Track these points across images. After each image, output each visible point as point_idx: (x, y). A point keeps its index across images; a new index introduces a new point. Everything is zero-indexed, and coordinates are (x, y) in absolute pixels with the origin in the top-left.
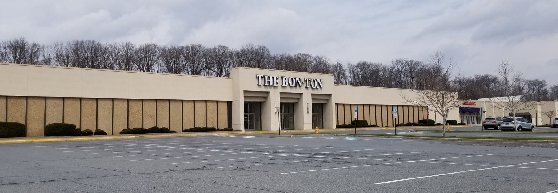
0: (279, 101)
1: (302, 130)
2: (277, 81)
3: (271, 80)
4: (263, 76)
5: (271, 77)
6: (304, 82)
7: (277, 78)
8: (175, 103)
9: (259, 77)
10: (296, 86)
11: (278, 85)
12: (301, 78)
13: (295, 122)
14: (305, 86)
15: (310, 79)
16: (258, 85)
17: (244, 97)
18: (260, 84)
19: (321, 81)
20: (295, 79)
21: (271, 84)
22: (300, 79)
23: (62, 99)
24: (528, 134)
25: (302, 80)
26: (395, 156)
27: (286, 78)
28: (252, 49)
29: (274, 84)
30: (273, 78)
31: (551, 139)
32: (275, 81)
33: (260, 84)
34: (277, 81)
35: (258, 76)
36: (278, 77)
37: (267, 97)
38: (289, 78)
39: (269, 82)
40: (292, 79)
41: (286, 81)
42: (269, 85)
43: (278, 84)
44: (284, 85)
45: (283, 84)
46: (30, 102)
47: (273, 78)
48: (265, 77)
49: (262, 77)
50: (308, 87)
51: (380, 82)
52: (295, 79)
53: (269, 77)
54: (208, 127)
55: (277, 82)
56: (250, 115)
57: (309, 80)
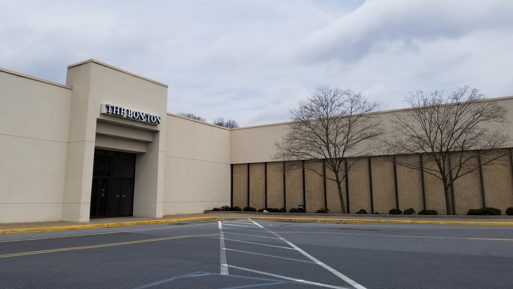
0: (95, 145)
1: (147, 218)
2: (124, 112)
3: (118, 110)
4: (112, 106)
7: (124, 110)
17: (98, 135)
19: (159, 118)
22: (142, 114)
24: (37, 224)
25: (144, 115)
27: (132, 111)
28: (465, 130)
30: (120, 109)
31: (201, 222)
34: (124, 112)
35: (147, 114)
37: (150, 142)
39: (117, 112)
41: (131, 113)
43: (124, 114)
46: (485, 159)
47: (120, 109)
51: (473, 151)
53: (117, 108)
54: (269, 207)
55: (123, 113)
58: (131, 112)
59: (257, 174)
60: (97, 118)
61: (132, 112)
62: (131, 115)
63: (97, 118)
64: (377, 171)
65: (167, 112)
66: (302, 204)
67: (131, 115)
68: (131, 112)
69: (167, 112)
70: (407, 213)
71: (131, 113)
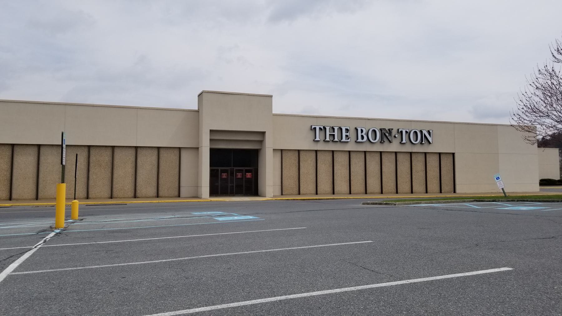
2: (348, 134)
4: (322, 127)
5: (336, 129)
6: (397, 136)
7: (347, 130)
8: (134, 158)
9: (315, 128)
10: (382, 142)
11: (349, 140)
12: (431, 131)
13: (334, 165)
14: (399, 140)
15: (408, 131)
16: (314, 140)
18: (317, 139)
19: (429, 133)
20: (421, 132)
21: (336, 139)
23: (178, 150)
26: (14, 260)
29: (342, 138)
30: (341, 129)
32: (344, 134)
33: (317, 139)
34: (348, 134)
35: (400, 130)
36: (349, 128)
38: (369, 130)
40: (416, 132)
41: (363, 134)
42: (324, 141)
43: (349, 139)
44: (360, 140)
45: (357, 139)
48: (325, 128)
49: (320, 129)
50: (404, 141)
52: (421, 132)
55: (347, 136)
56: (221, 170)
57: (406, 132)
58: (362, 131)
59: (168, 159)
60: (265, 132)
61: (364, 132)
62: (363, 137)
63: (265, 132)
64: (18, 159)
65: (273, 113)
66: (61, 144)
67: (363, 137)
68: (362, 131)
69: (273, 113)
70: (281, 251)
71: (363, 134)
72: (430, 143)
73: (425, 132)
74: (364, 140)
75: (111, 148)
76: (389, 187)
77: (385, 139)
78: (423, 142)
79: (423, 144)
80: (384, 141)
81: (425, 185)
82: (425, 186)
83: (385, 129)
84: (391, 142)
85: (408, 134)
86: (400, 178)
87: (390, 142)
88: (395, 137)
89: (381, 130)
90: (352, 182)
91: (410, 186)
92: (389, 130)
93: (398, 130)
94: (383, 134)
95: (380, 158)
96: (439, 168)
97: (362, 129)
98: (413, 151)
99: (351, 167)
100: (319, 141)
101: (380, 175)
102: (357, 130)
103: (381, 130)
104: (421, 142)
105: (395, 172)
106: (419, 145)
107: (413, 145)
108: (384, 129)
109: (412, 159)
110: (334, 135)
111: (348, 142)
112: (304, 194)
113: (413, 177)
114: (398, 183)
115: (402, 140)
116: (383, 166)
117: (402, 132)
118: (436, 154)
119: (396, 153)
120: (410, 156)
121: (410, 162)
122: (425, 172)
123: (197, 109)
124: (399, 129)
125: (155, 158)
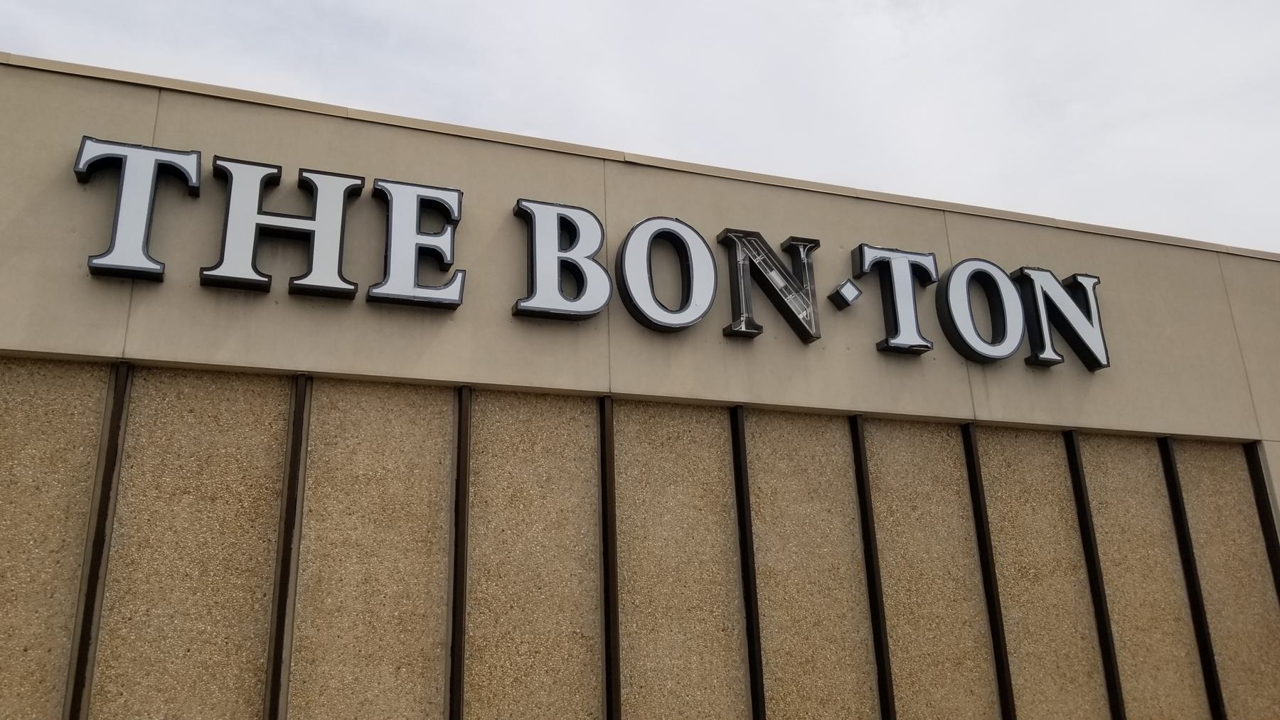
5: (331, 194)
6: (849, 292)
12: (1087, 283)
15: (927, 262)
19: (1074, 288)
20: (1022, 281)
34: (442, 242)
35: (870, 256)
36: (451, 199)
41: (578, 254)
50: (908, 336)
52: (1022, 281)
57: (920, 275)
58: (568, 232)
62: (572, 277)
67: (572, 277)
68: (568, 232)
72: (1090, 362)
73: (1045, 283)
74: (588, 303)
75: (104, 374)
76: (823, 703)
77: (762, 313)
78: (1048, 354)
79: (1048, 364)
80: (750, 323)
81: (1099, 678)
82: (1103, 691)
83: (757, 235)
84: (813, 331)
85: (932, 288)
86: (908, 629)
87: (804, 336)
88: (838, 301)
89: (727, 242)
90: (474, 671)
91: (994, 687)
92: (791, 248)
93: (859, 253)
94: (744, 281)
95: (729, 458)
96: (1174, 548)
97: (576, 216)
98: (984, 415)
99: (476, 529)
100: (150, 279)
101: (737, 602)
102: (524, 217)
103: (727, 242)
104: (1027, 353)
105: (863, 576)
106: (1018, 376)
107: (976, 373)
108: (751, 237)
109: (984, 471)
110: (304, 240)
111: (447, 308)
112: (1152, 439)
113: (1010, 616)
114: (895, 668)
115: (892, 326)
116: (757, 527)
117: (883, 269)
118: (1140, 449)
119: (855, 423)
120: (727, 434)
121: (967, 499)
122: (1083, 574)
123: (457, 299)
124: (861, 248)
125: (589, 438)
